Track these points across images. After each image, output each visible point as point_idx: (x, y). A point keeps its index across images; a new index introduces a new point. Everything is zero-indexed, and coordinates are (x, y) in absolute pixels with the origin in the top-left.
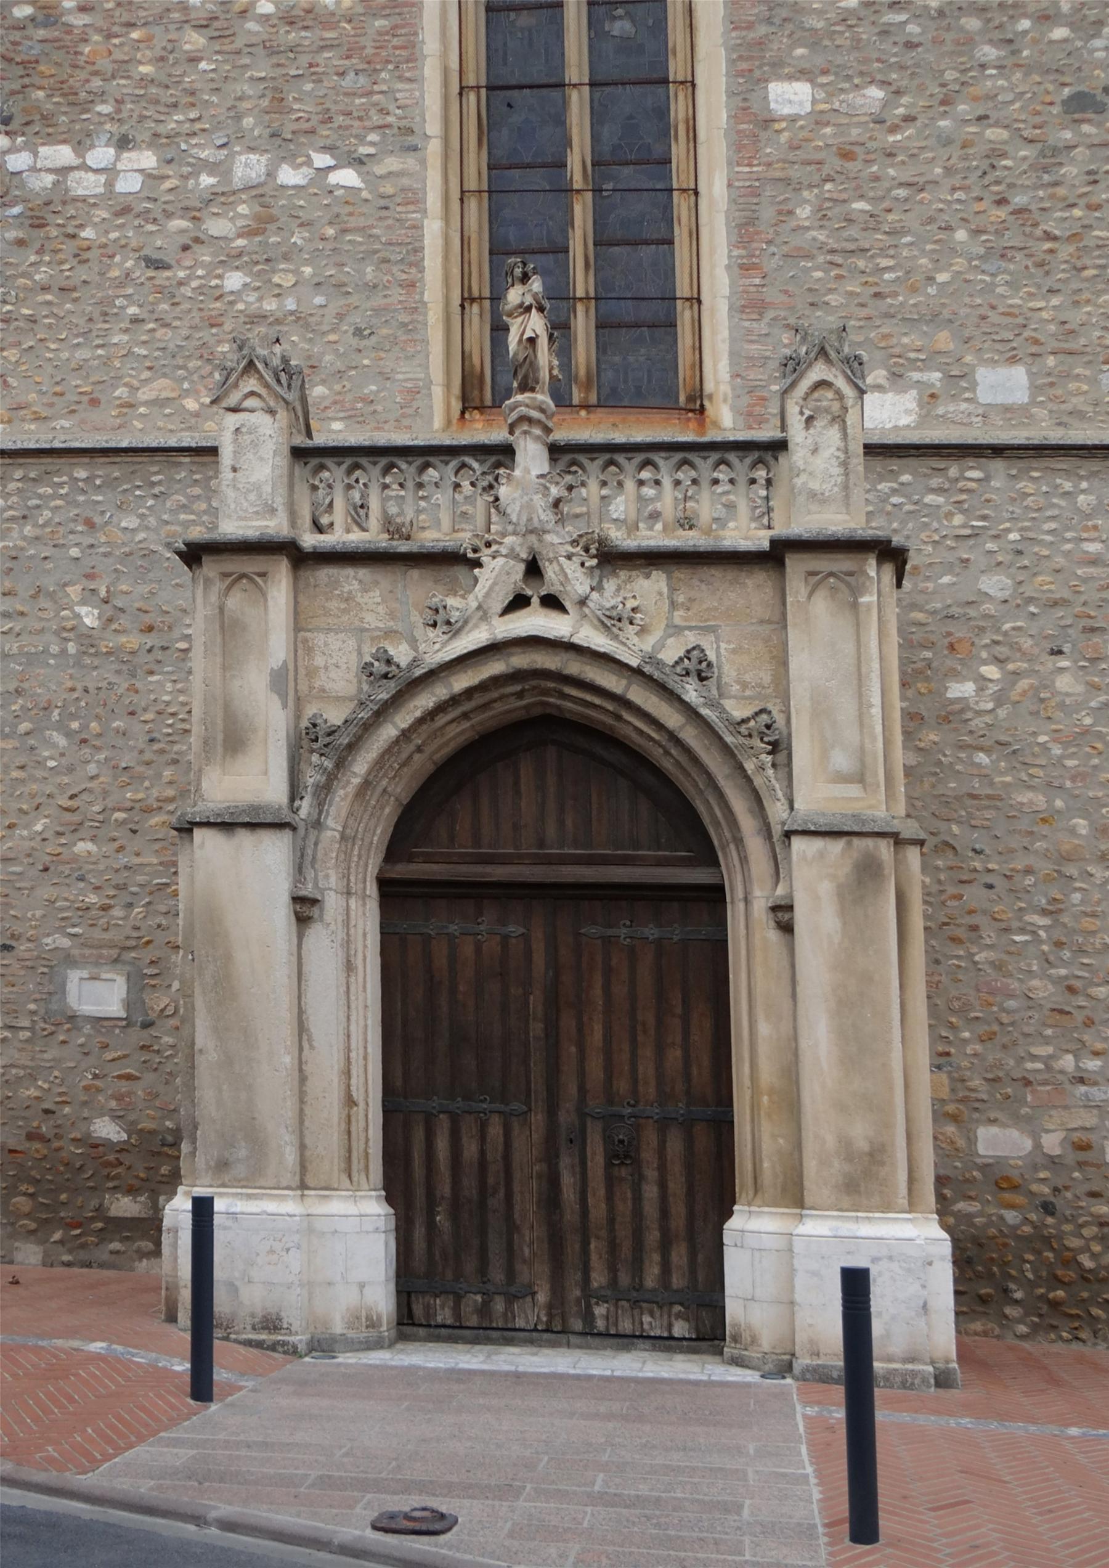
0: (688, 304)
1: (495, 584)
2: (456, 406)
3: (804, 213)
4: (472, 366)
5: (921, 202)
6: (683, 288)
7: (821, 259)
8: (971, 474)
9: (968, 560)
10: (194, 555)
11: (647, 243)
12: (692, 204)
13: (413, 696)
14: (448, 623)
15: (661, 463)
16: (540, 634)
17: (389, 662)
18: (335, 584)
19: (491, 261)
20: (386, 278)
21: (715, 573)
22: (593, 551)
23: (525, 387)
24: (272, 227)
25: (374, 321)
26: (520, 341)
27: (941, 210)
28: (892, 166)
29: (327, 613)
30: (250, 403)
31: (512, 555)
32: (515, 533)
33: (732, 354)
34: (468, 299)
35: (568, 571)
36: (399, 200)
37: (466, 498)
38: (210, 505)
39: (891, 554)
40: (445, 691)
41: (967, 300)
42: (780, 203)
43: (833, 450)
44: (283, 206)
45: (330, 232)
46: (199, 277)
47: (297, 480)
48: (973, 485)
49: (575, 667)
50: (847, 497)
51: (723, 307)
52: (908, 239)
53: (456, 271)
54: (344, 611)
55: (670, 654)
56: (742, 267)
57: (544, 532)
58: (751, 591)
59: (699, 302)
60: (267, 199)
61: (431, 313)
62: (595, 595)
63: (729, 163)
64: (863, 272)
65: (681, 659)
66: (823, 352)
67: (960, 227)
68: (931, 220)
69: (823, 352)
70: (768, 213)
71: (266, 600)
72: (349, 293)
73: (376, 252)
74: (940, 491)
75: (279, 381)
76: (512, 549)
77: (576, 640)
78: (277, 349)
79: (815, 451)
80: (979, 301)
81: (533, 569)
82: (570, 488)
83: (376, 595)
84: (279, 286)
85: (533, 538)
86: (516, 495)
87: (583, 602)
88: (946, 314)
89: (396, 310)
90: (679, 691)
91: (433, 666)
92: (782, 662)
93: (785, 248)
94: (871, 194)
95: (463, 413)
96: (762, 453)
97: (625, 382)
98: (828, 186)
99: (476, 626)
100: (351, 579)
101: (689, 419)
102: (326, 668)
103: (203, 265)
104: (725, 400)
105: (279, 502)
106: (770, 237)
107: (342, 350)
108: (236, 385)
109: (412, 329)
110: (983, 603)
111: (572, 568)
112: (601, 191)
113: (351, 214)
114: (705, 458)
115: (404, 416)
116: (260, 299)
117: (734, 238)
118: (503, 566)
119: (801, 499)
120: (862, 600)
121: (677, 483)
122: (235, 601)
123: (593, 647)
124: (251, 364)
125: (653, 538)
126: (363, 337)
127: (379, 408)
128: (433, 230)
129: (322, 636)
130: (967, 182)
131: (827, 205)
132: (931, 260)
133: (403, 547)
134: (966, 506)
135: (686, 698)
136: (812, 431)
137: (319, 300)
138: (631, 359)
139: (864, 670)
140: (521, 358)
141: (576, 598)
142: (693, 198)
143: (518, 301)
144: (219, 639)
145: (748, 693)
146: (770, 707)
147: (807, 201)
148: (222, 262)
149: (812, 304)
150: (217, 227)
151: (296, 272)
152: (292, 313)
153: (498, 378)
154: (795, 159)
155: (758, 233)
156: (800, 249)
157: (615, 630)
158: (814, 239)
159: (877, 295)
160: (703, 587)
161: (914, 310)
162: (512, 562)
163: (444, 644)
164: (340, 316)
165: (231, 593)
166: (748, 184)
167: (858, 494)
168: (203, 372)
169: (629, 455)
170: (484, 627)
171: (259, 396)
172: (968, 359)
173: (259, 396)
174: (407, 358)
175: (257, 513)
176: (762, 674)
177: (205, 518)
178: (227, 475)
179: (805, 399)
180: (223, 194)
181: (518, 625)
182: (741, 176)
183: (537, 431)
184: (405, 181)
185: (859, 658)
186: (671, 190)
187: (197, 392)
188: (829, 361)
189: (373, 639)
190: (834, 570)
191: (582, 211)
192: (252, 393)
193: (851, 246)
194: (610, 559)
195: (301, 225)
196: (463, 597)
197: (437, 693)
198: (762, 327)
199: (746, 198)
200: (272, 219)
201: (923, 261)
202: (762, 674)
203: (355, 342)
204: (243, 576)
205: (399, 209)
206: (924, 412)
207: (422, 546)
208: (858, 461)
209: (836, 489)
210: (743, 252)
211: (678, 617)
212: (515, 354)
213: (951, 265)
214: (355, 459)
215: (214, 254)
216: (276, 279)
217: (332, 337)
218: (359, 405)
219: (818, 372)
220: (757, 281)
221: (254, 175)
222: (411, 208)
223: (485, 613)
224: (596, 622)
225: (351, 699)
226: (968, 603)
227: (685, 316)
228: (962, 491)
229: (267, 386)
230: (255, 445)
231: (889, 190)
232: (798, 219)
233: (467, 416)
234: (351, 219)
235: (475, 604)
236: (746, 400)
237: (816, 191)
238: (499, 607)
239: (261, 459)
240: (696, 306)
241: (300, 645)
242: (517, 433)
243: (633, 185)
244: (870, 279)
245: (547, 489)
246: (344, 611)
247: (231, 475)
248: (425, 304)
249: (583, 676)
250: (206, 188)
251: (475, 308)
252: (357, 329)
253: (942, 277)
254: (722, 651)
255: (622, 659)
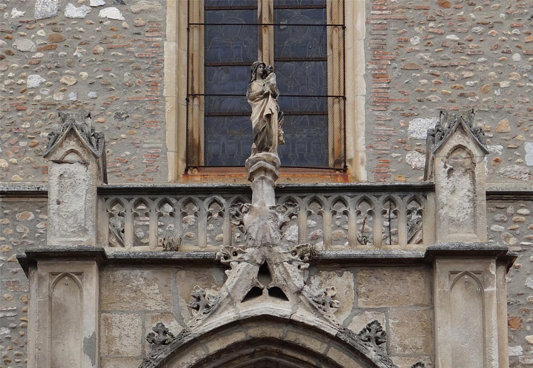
0: (337, 100)
1: (240, 280)
2: (183, 166)
3: (415, 41)
4: (193, 140)
5: (491, 35)
6: (333, 89)
7: (426, 71)
8: (521, 211)
9: (519, 267)
10: (30, 261)
11: (309, 60)
12: (341, 35)
13: (181, 356)
14: (207, 306)
15: (348, 200)
16: (270, 314)
17: (165, 333)
18: (127, 280)
19: (205, 71)
20: (137, 80)
21: (386, 273)
22: (306, 258)
23: (261, 148)
24: (61, 45)
25: (129, 108)
26: (261, 116)
27: (504, 41)
28: (472, 11)
29: (121, 300)
30: (71, 157)
31: (252, 261)
32: (253, 246)
33: (367, 132)
34: (191, 96)
35: (290, 271)
36: (147, 29)
37: (189, 226)
38: (15, 231)
39: (505, 259)
40: (203, 353)
41: (520, 99)
42: (399, 35)
43: (465, 191)
44: (68, 31)
45: (101, 49)
46: (10, 78)
47: (100, 210)
48: (523, 218)
49: (292, 336)
50: (475, 222)
51: (362, 102)
52: (483, 59)
53: (184, 77)
54: (134, 299)
55: (357, 326)
56: (374, 76)
57: (274, 245)
58: (412, 284)
59: (344, 98)
60: (57, 26)
61: (168, 104)
62: (307, 288)
63: (367, 8)
64: (453, 80)
65: (365, 330)
66: (460, 127)
67: (516, 52)
68: (497, 47)
69: (460, 127)
70: (392, 41)
71: (81, 291)
72: (112, 90)
73: (132, 63)
74: (501, 222)
75: (91, 143)
76: (252, 257)
77: (294, 318)
78: (89, 121)
79: (453, 192)
80: (527, 100)
81: (265, 270)
82: (291, 216)
83: (155, 288)
84: (65, 84)
85: (265, 249)
86: (255, 220)
87: (299, 292)
88: (506, 107)
89: (144, 102)
90: (364, 351)
91: (197, 336)
92: (431, 331)
93: (403, 64)
94: (459, 30)
95: (186, 171)
96: (416, 194)
97: (293, 151)
98: (431, 24)
99: (226, 309)
100: (138, 277)
101: (337, 175)
102: (120, 337)
103: (13, 70)
104: (362, 163)
105: (89, 225)
106: (393, 56)
107: (107, 128)
108: (61, 145)
109: (155, 114)
110: (528, 294)
111: (292, 269)
112: (279, 25)
113: (115, 37)
114: (378, 197)
115: (148, 172)
116: (52, 93)
117: (370, 57)
118: (245, 268)
119: (445, 224)
120: (486, 290)
121: (359, 213)
122: (59, 292)
123: (306, 322)
124: (72, 130)
125: (343, 250)
126: (122, 119)
127: (132, 167)
128: (171, 50)
129: (118, 316)
130: (521, 23)
131: (430, 36)
132: (498, 73)
133: (176, 256)
134: (518, 232)
135: (368, 356)
136: (451, 179)
137: (92, 94)
138: (297, 136)
139: (487, 336)
140: (261, 128)
141: (295, 290)
142: (341, 31)
143: (259, 90)
144: (48, 318)
145: (407, 352)
146: (421, 361)
147: (417, 34)
148: (26, 68)
149: (420, 101)
150: (23, 44)
151: (77, 75)
152: (73, 102)
153: (209, 148)
154: (410, 6)
155: (385, 54)
156: (412, 65)
157: (320, 310)
158: (422, 58)
159: (462, 95)
160: (378, 282)
161: (486, 105)
162: (251, 266)
163: (205, 321)
164: (106, 105)
165: (57, 286)
166: (379, 22)
167: (483, 220)
168: (12, 141)
169: (327, 195)
170: (231, 309)
171: (77, 153)
172: (520, 137)
173: (77, 153)
174: (151, 133)
175: (73, 232)
176: (417, 340)
177: (12, 239)
178: (53, 206)
179: (447, 158)
180: (28, 22)
181: (254, 308)
182: (375, 17)
183: (270, 178)
184: (152, 16)
185: (484, 329)
186: (326, 25)
187: (7, 154)
188: (464, 132)
189: (153, 318)
190: (468, 270)
191: (267, 38)
192: (72, 151)
193: (445, 63)
194: (318, 264)
195: (81, 44)
196: (215, 289)
197: (200, 353)
198: (387, 115)
199: (378, 31)
200: (61, 40)
201: (492, 73)
202: (417, 340)
203: (115, 122)
204: (66, 275)
205: (147, 34)
206: (491, 171)
207: (189, 255)
208: (482, 199)
209: (467, 217)
210: (375, 66)
211: (361, 302)
212: (257, 126)
213: (510, 76)
214: (140, 196)
215: (20, 63)
216: (63, 80)
217: (100, 119)
218: (118, 165)
219: (457, 139)
220: (384, 85)
221: (49, 10)
222: (156, 34)
223: (232, 300)
224: (308, 305)
225: (137, 359)
226: (519, 295)
227: (334, 108)
228: (515, 222)
229: (83, 146)
230: (73, 186)
231: (471, 27)
232: (412, 45)
233: (189, 172)
234: (115, 40)
235: (226, 294)
236: (376, 163)
237: (423, 27)
238: (241, 295)
239: (77, 195)
240: (342, 102)
241: (102, 322)
242: (256, 179)
243: (301, 22)
244: (457, 85)
245: (276, 216)
246: (134, 299)
247: (57, 206)
248: (164, 97)
249: (297, 342)
250: (17, 18)
251: (196, 101)
252: (117, 114)
253: (504, 84)
254: (390, 324)
255: (326, 330)
